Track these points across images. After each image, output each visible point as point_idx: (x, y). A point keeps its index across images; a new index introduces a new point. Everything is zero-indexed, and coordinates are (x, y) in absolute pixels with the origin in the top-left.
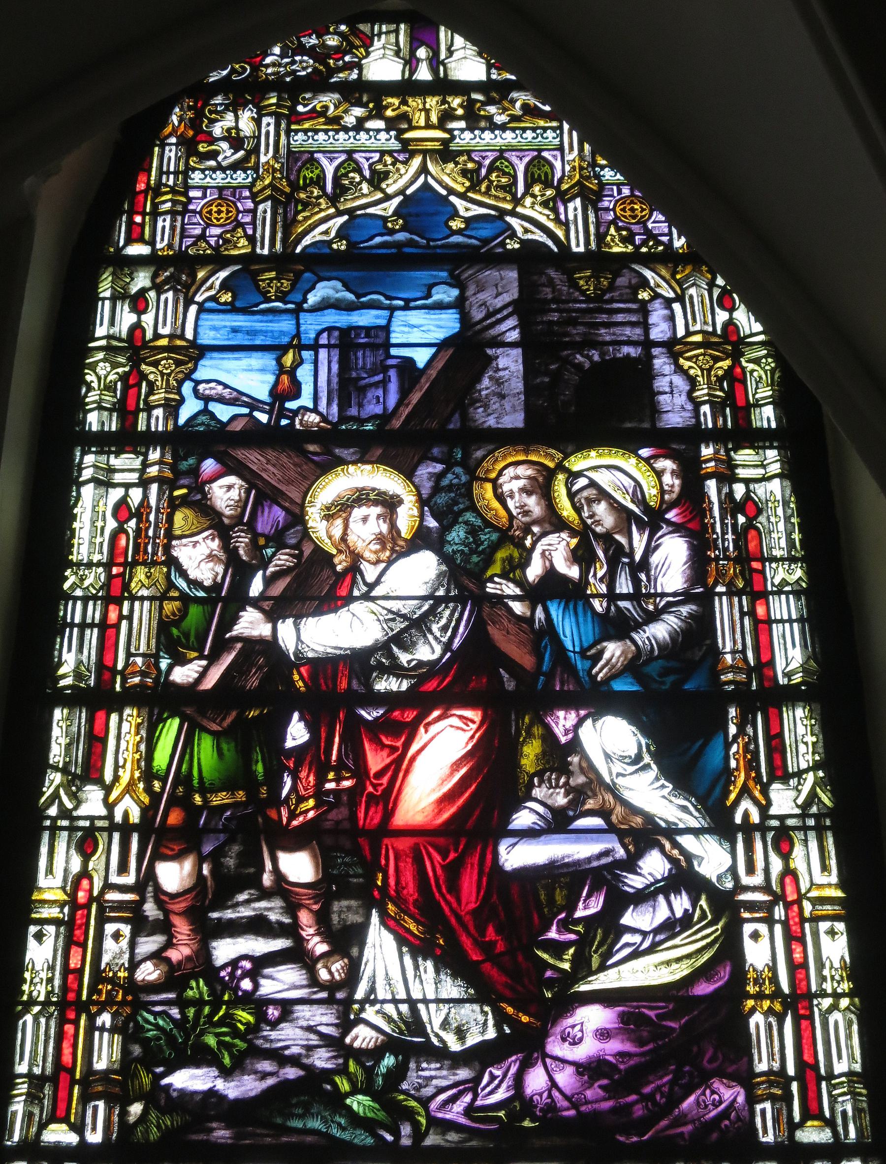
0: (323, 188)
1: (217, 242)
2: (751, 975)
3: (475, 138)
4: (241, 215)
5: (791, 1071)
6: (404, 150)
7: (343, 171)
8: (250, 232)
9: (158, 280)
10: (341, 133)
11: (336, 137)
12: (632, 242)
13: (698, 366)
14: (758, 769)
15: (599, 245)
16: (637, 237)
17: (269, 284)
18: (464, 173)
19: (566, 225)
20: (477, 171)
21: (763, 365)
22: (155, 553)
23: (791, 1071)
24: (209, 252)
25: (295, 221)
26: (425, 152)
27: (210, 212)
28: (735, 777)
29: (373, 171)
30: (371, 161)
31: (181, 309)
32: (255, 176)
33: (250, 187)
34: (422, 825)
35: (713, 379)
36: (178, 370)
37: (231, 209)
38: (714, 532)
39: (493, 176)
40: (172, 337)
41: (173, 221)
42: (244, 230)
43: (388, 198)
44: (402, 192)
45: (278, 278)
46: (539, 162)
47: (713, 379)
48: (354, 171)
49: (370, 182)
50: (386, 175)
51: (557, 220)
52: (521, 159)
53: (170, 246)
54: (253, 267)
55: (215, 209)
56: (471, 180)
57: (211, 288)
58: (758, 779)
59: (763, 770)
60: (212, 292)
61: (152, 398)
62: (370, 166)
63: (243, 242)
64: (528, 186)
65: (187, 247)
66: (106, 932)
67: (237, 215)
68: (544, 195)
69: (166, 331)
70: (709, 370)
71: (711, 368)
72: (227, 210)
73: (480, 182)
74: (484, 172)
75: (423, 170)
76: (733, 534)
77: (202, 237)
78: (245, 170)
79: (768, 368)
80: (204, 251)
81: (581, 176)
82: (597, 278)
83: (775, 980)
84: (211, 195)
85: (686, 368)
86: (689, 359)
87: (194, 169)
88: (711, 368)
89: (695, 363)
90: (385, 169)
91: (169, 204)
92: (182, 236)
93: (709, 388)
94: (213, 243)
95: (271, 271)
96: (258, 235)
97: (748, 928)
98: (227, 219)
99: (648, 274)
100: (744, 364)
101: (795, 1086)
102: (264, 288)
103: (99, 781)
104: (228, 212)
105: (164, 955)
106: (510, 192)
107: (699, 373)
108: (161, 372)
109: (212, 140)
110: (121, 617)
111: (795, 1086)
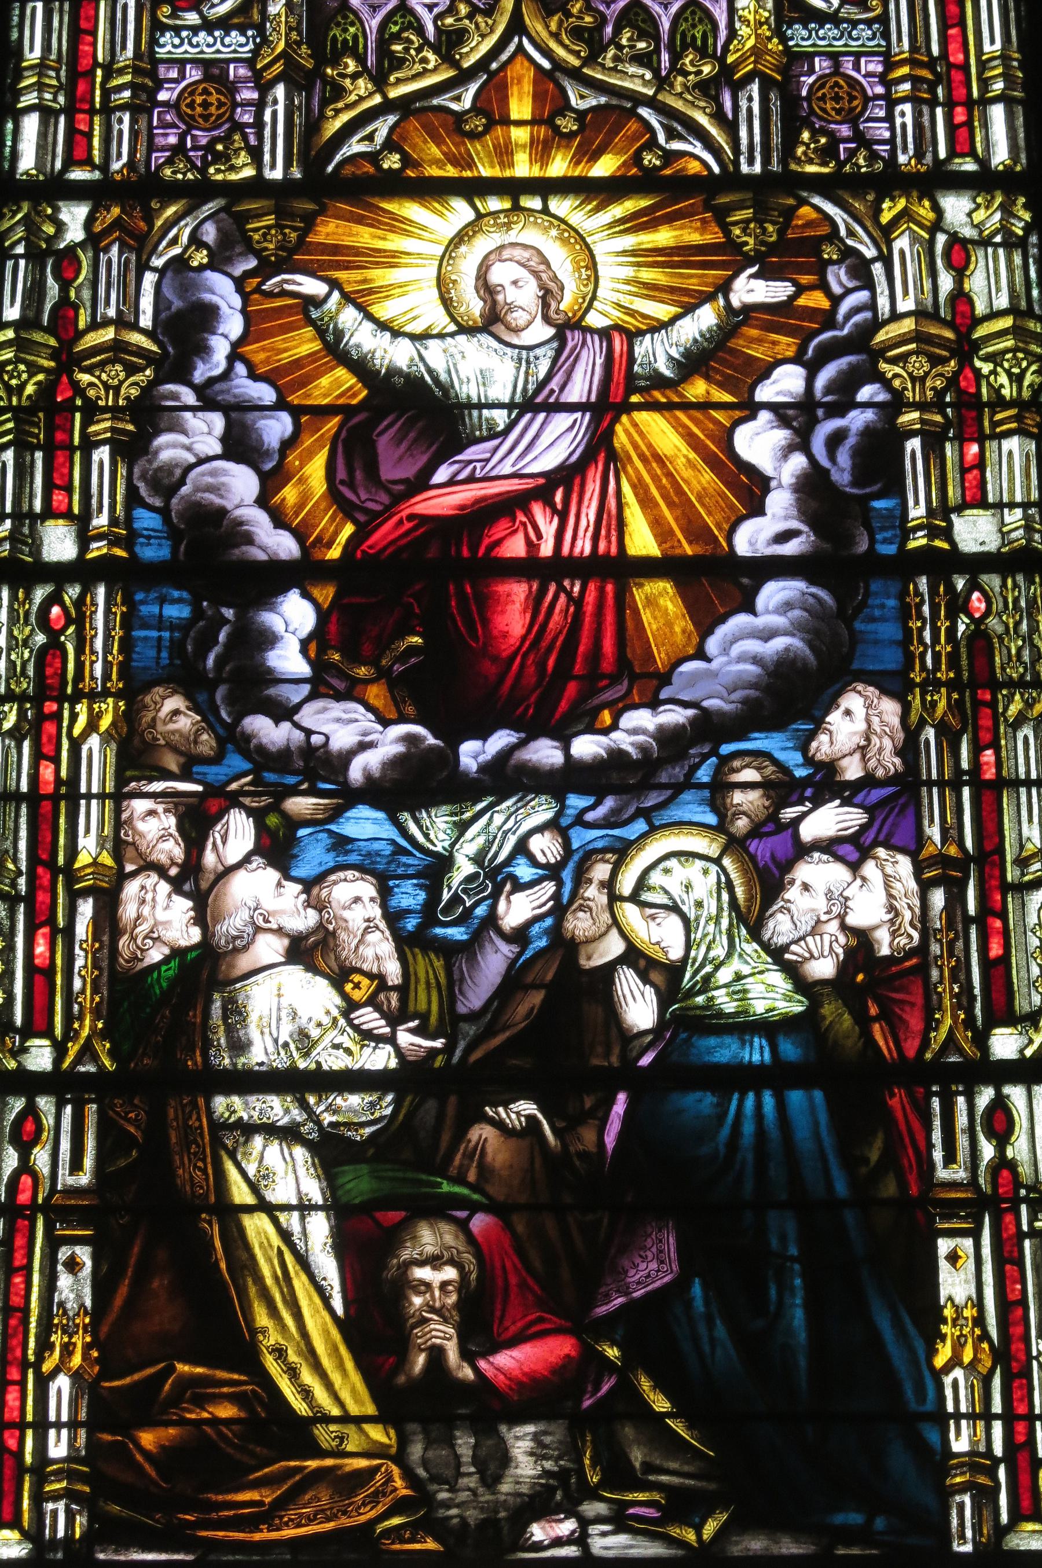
2: (948, 1312)
4: (239, 110)
5: (998, 1450)
7: (395, 29)
8: (253, 141)
9: (98, 228)
10: (202, 34)
11: (194, 40)
12: (835, 155)
15: (784, 162)
16: (842, 146)
17: (264, 235)
18: (577, 33)
19: (731, 128)
21: (1006, 365)
22: (107, 676)
23: (998, 1450)
24: (190, 176)
27: (191, 105)
30: (436, 11)
31: (132, 276)
32: (258, 40)
34: (225, 884)
36: (132, 379)
42: (245, 137)
45: (278, 226)
46: (693, 13)
48: (409, 27)
51: (718, 116)
52: (666, 8)
53: (131, 164)
56: (589, 43)
57: (174, 242)
59: (978, 1011)
60: (177, 251)
61: (93, 429)
63: (243, 158)
65: (159, 167)
67: (233, 112)
68: (700, 72)
69: (906, 305)
70: (923, 379)
71: (927, 374)
72: (193, 109)
77: (179, 149)
78: (242, 30)
80: (184, 174)
82: (761, 223)
83: (980, 1321)
84: (194, 74)
85: (889, 375)
86: (89, 370)
87: (164, 28)
89: (99, 378)
90: (459, 25)
91: (127, 94)
92: (151, 148)
97: (944, 1246)
100: (978, 364)
101: (1002, 1473)
102: (258, 242)
103: (48, 1033)
105: (30, 1118)
106: (648, 65)
108: (105, 384)
111: (1002, 1473)
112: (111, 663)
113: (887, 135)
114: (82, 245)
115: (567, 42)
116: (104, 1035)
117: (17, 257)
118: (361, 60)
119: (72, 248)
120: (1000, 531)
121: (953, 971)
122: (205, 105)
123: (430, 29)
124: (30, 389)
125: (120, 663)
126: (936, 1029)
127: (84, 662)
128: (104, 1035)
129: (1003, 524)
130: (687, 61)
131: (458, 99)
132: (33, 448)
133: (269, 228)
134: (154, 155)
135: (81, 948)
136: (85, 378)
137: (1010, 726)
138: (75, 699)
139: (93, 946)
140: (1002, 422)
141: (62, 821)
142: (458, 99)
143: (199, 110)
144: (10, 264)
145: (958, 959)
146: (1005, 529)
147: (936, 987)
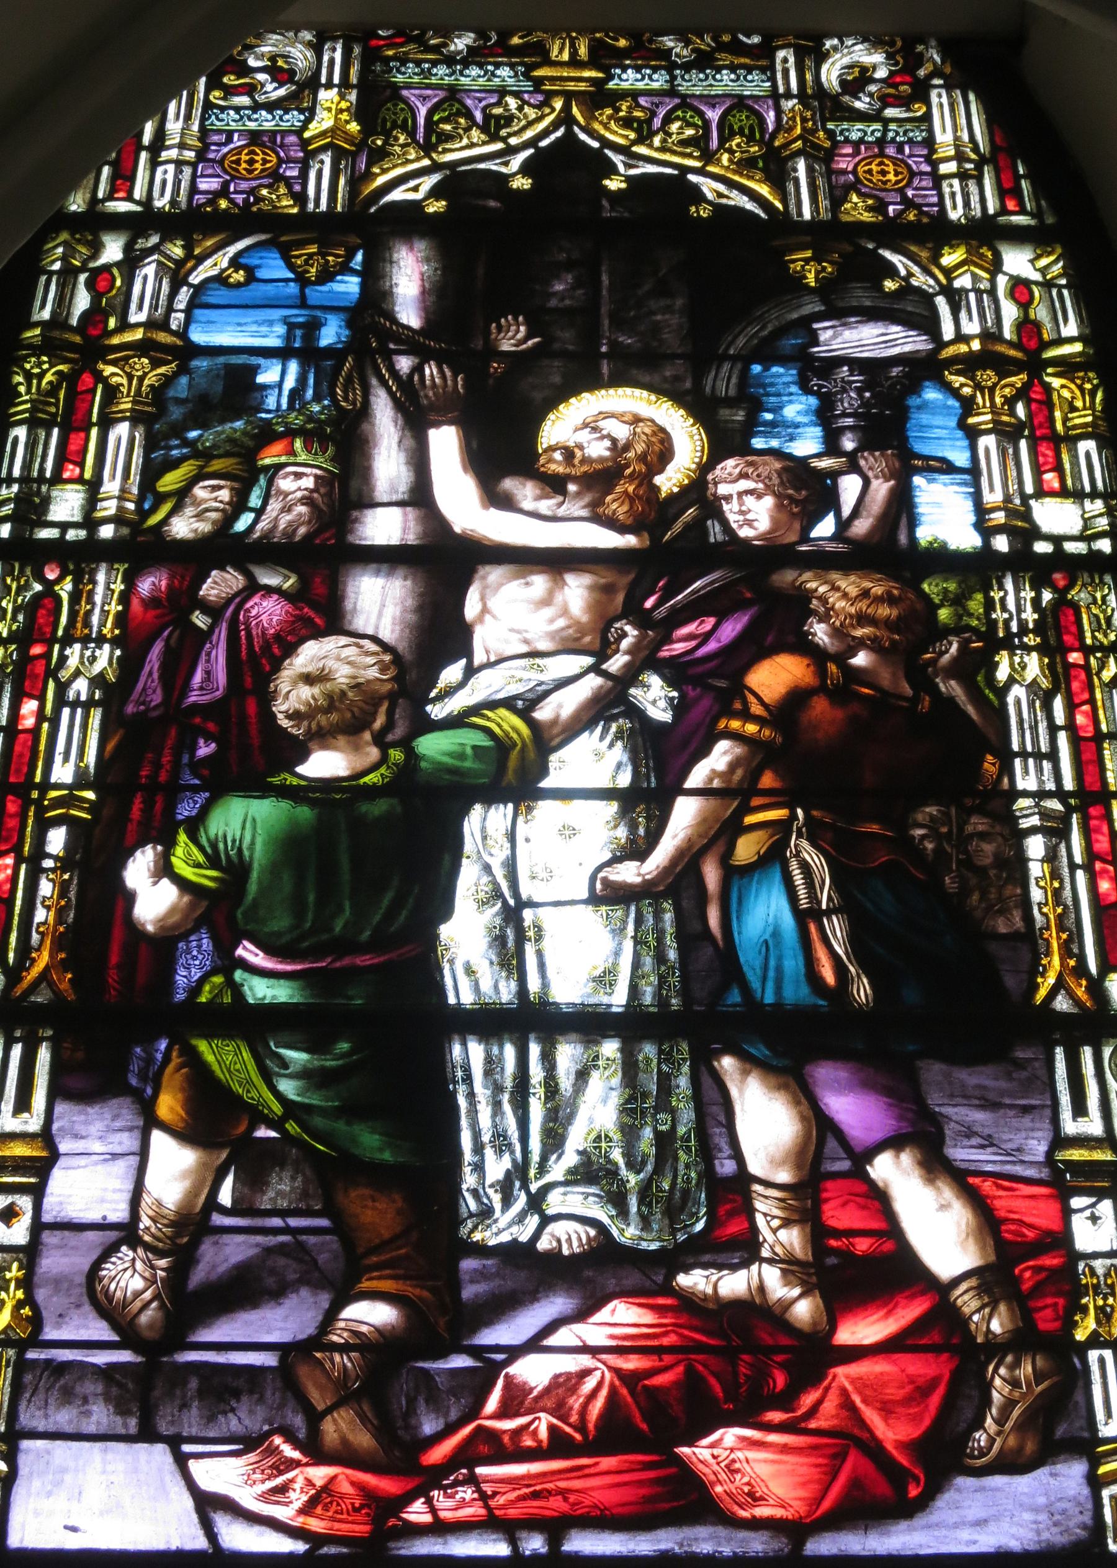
0: (412, 134)
1: (246, 200)
3: (643, 79)
6: (537, 89)
8: (297, 188)
13: (125, 372)
14: (1082, 958)
17: (306, 261)
20: (649, 121)
25: (369, 176)
26: (568, 96)
28: (1044, 966)
29: (487, 117)
33: (299, 132)
35: (998, 400)
37: (900, 170)
38: (1004, 608)
39: (674, 127)
40: (150, 325)
41: (179, 171)
43: (512, 151)
44: (532, 142)
47: (998, 400)
49: (484, 129)
50: (509, 119)
54: (283, 239)
55: (244, 157)
58: (1081, 970)
62: (484, 110)
64: (723, 140)
66: (17, 1197)
71: (995, 385)
72: (263, 159)
73: (652, 134)
74: (657, 123)
75: (566, 119)
76: (1035, 611)
79: (1088, 386)
81: (803, 129)
86: (114, 363)
88: (995, 385)
89: (122, 369)
93: (992, 412)
94: (240, 202)
95: (808, 249)
96: (311, 191)
98: (263, 170)
99: (895, 259)
104: (265, 161)
107: (125, 381)
109: (247, 71)
110: (40, 716)
112: (113, 591)
113: (935, 200)
114: (117, 264)
115: (616, 129)
116: (65, 965)
117: (51, 273)
118: (412, 134)
119: (107, 268)
120: (1082, 516)
121: (1060, 918)
122: (251, 162)
123: (478, 116)
124: (49, 377)
125: (121, 592)
126: (1043, 975)
127: (78, 612)
128: (65, 965)
129: (1084, 512)
130: (734, 143)
131: (506, 164)
132: (48, 426)
133: (310, 256)
134: (197, 197)
135: (38, 932)
136: (109, 370)
137: (1107, 685)
138: (68, 640)
139: (58, 903)
140: (1075, 427)
141: (40, 764)
142: (506, 164)
143: (244, 165)
144: (44, 278)
145: (1066, 907)
146: (1086, 516)
147: (1042, 934)
